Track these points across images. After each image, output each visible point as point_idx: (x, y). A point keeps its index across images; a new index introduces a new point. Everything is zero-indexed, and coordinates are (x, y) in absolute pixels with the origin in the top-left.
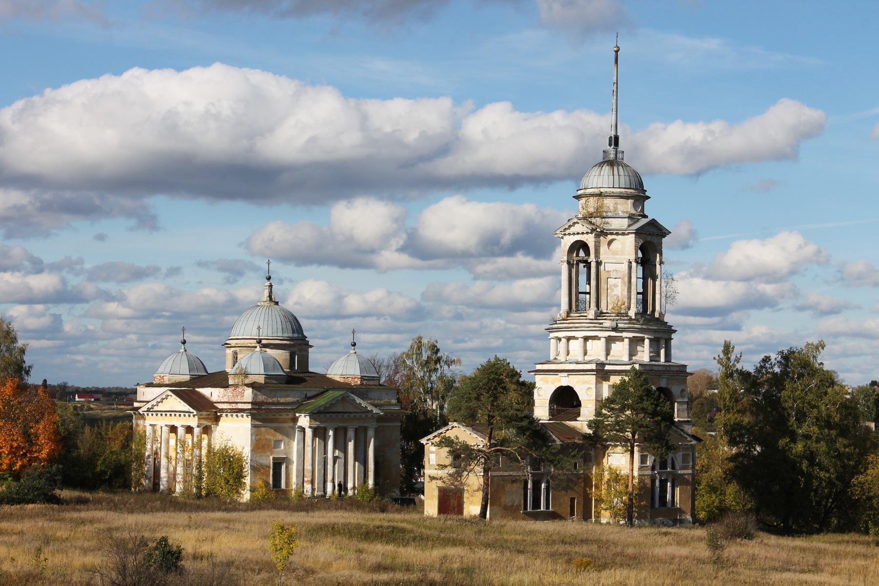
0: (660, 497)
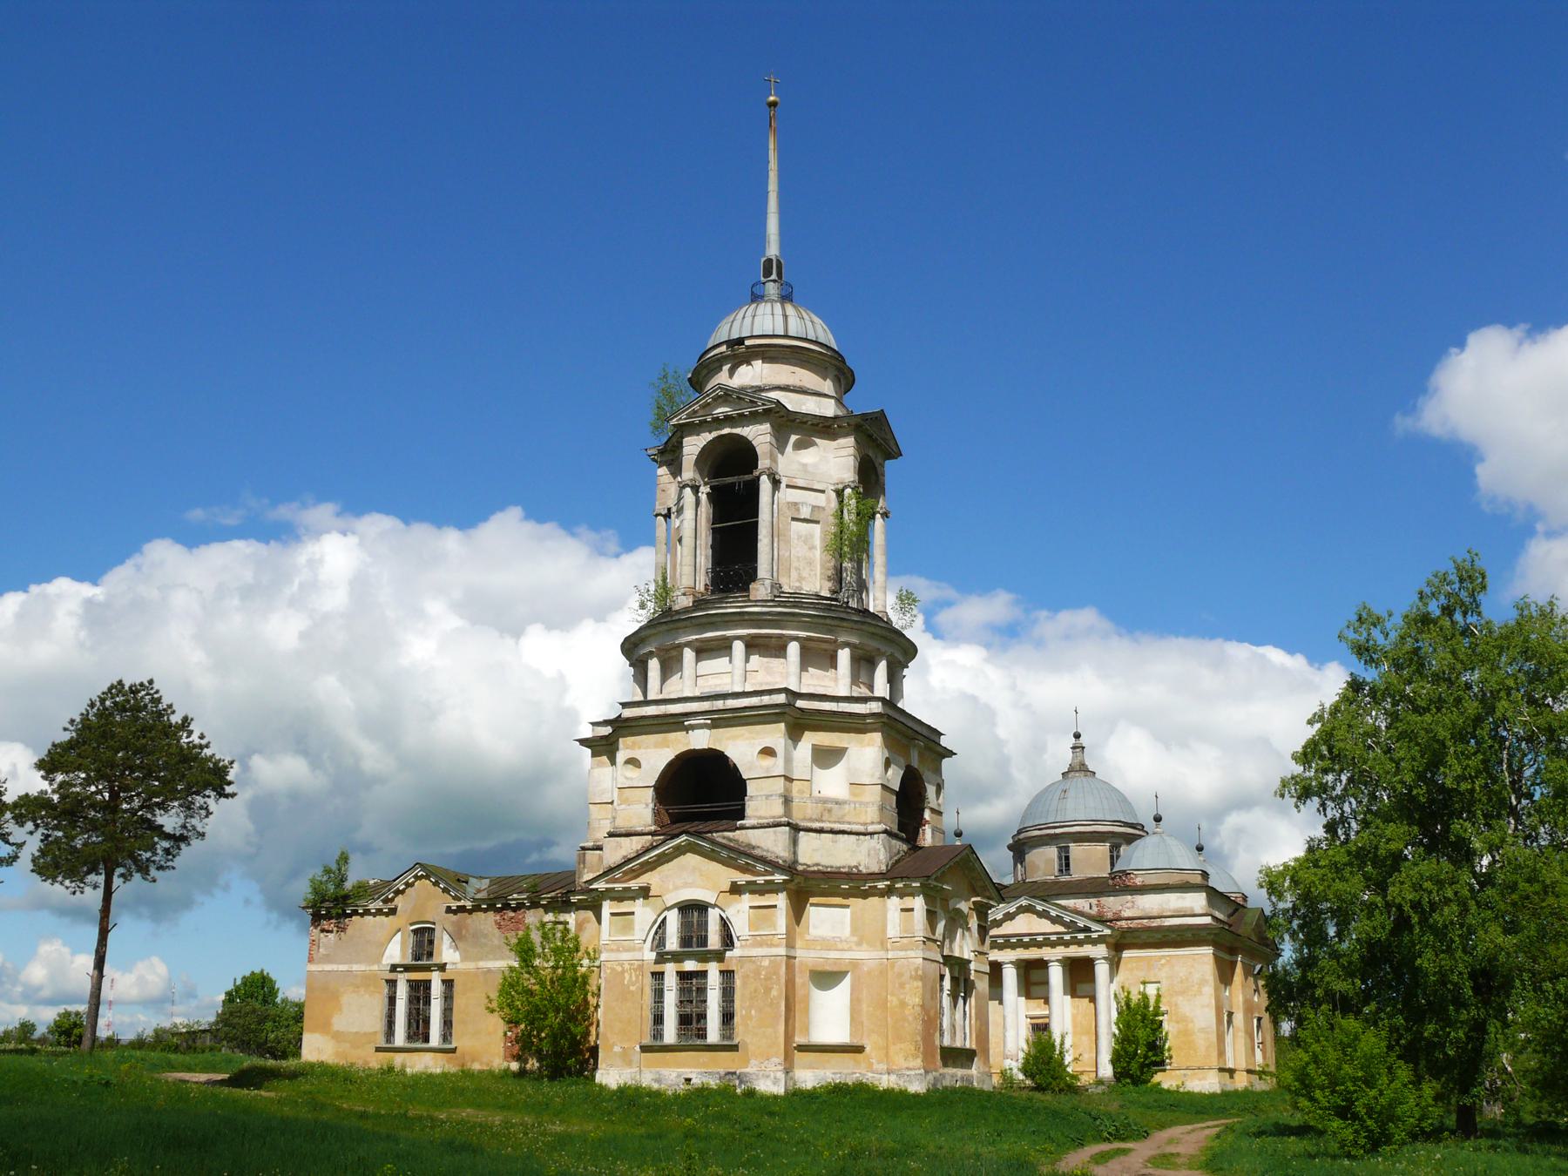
0: (428, 1002)
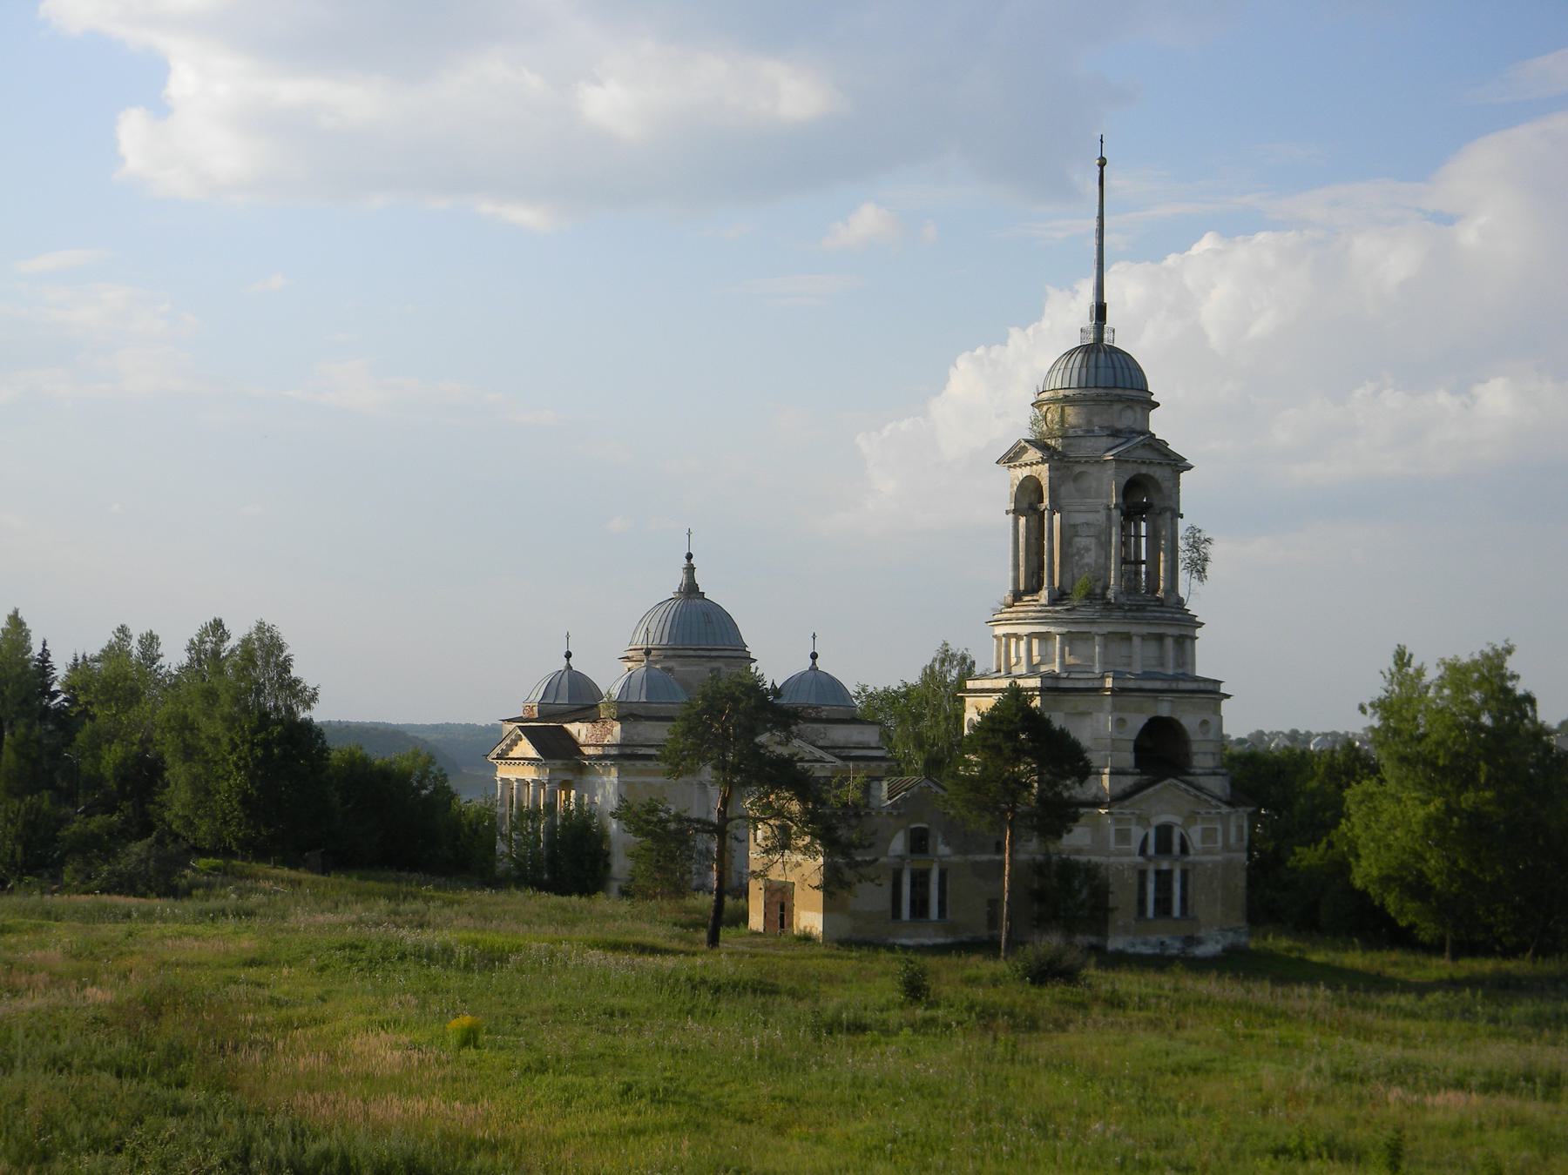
0: (1157, 901)
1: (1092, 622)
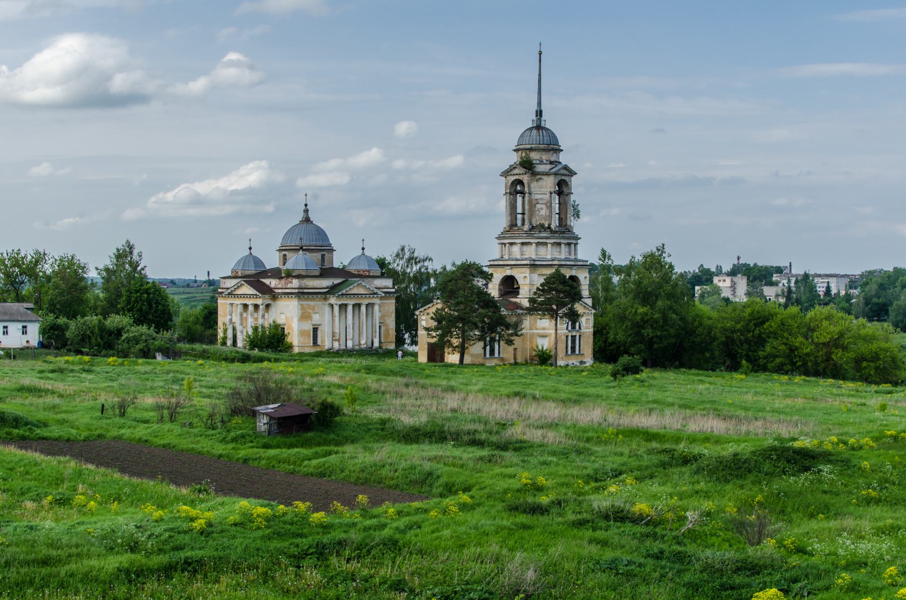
1: (547, 238)
